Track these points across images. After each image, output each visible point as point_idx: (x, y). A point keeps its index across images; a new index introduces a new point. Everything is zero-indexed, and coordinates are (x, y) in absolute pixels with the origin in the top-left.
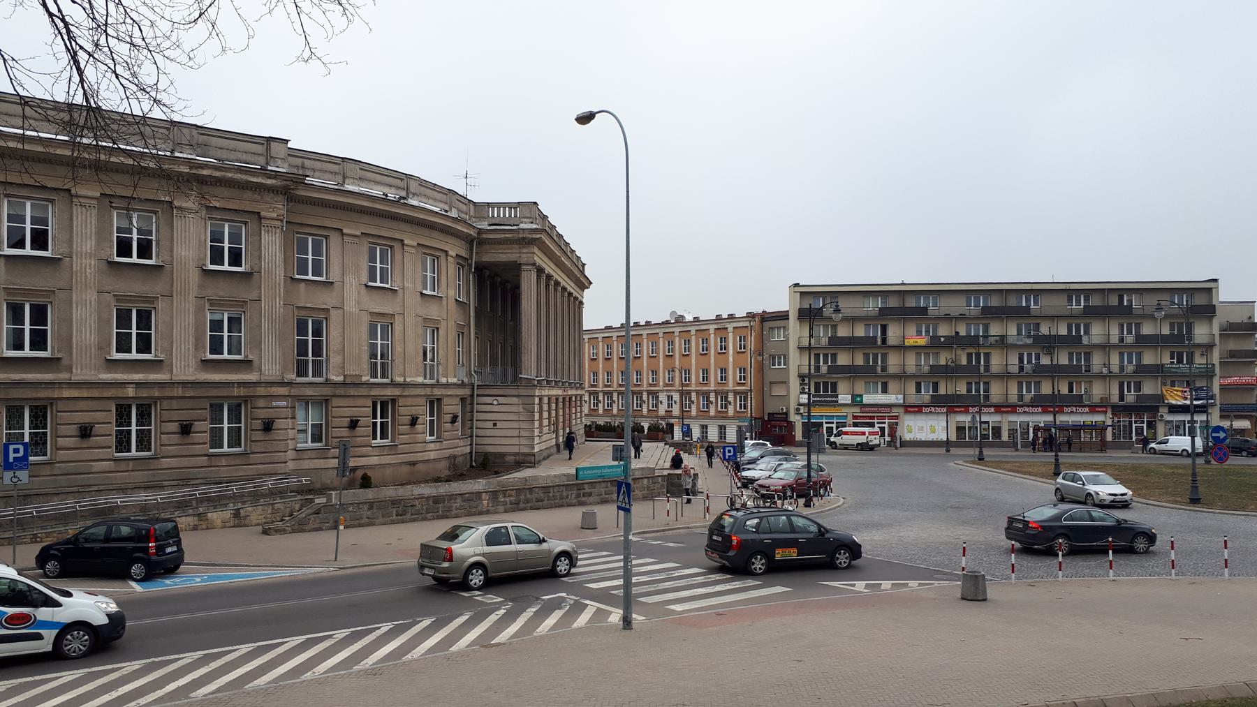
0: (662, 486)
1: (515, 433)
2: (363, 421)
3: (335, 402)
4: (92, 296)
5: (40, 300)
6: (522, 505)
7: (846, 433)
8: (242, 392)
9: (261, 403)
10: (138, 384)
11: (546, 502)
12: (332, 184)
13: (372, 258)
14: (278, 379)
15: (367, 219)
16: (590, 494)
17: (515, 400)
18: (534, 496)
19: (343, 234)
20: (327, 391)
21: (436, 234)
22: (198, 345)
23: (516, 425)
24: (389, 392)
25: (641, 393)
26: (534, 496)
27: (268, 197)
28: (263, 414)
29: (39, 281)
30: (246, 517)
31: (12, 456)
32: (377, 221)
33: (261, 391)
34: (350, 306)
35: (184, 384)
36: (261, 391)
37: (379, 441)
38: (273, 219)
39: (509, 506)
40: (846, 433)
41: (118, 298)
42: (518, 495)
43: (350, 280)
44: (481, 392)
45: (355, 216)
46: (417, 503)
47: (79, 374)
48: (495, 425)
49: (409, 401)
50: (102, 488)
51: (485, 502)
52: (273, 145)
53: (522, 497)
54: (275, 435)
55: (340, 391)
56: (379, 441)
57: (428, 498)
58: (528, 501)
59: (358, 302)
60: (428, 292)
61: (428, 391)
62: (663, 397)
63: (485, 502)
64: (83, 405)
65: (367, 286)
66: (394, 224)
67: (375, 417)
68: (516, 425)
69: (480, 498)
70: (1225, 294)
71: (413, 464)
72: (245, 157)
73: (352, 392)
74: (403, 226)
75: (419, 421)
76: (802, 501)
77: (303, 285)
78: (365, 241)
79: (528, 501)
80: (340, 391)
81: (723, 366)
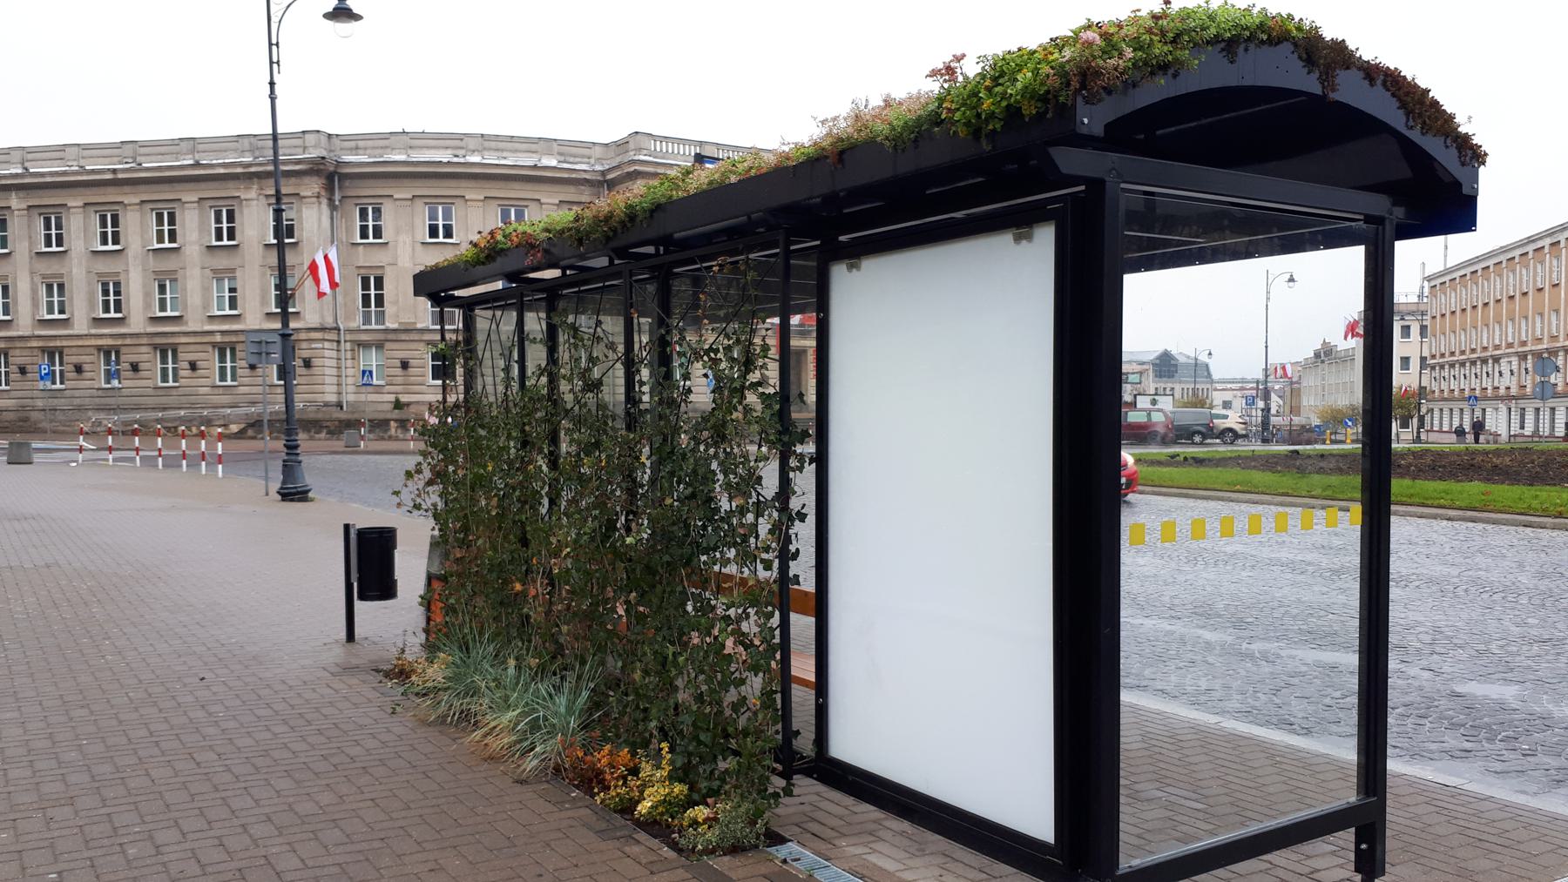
3: (388, 345)
4: (197, 272)
5: (379, 272)
9: (304, 345)
10: (223, 332)
12: (402, 158)
15: (142, 188)
21: (516, 185)
22: (92, 306)
27: (307, 180)
29: (169, 264)
32: (501, 184)
35: (195, 333)
41: (44, 276)
45: (406, 182)
47: (192, 326)
49: (17, 352)
54: (315, 370)
55: (391, 336)
64: (192, 348)
73: (403, 337)
74: (464, 183)
78: (419, 203)
80: (391, 336)
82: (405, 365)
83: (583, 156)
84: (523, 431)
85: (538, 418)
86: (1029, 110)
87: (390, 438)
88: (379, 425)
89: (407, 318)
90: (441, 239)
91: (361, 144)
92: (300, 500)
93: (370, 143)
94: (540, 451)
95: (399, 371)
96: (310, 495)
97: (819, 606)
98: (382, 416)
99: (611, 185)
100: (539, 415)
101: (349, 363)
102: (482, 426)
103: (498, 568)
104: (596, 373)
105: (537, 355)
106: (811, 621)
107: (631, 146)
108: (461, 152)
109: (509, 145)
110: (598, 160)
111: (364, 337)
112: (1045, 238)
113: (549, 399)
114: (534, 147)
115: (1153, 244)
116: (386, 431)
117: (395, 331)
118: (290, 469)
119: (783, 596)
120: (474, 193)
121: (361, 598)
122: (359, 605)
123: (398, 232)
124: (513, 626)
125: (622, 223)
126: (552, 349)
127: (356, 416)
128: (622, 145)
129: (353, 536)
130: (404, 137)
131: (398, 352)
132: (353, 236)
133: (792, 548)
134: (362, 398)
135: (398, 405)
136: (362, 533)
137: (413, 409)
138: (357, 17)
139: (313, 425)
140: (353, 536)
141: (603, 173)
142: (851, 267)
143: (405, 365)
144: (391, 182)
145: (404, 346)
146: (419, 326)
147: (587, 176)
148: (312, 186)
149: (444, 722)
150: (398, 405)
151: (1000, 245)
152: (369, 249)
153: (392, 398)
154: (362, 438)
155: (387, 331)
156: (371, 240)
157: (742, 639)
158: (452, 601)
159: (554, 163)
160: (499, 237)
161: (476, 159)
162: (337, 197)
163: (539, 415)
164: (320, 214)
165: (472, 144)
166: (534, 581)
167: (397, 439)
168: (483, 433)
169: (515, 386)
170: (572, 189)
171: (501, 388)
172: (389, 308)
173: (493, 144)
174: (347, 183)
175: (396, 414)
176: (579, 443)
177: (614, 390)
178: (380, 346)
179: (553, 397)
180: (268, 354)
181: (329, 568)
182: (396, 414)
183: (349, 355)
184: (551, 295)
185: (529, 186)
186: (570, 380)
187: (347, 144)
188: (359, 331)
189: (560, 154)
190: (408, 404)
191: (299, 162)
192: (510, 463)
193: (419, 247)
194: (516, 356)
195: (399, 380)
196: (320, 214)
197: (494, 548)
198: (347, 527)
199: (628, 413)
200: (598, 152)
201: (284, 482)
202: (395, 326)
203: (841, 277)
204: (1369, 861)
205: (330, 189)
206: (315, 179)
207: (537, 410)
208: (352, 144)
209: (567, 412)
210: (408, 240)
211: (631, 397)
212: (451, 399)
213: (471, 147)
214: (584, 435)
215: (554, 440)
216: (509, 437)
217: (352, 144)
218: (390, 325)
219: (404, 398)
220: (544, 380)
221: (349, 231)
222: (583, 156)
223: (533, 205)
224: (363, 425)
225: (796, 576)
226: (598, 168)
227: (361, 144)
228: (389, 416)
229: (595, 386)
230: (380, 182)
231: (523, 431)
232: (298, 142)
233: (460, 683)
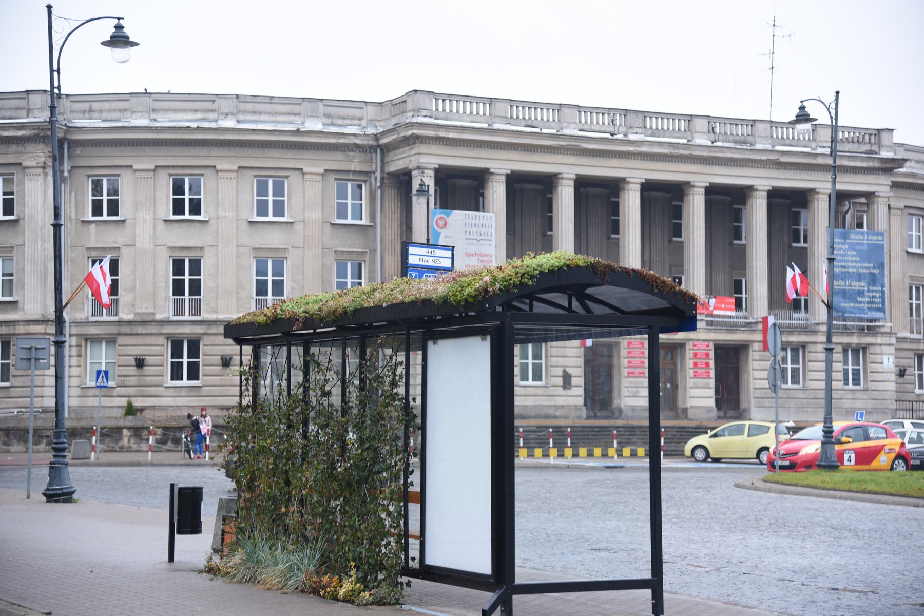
3: (121, 340)
7: (829, 363)
12: (144, 122)
13: (342, 194)
14: (38, 317)
19: (304, 174)
20: (113, 330)
21: (276, 153)
27: (30, 147)
32: (258, 152)
34: (144, 240)
37: (185, 382)
38: (34, 167)
40: (829, 363)
43: (145, 216)
45: (148, 150)
52: (31, 96)
56: (185, 382)
59: (154, 237)
60: (914, 250)
65: (907, 252)
66: (203, 151)
69: (121, 433)
70: (125, 30)
72: (8, 114)
73: (140, 330)
74: (215, 151)
76: (538, 452)
77: (93, 226)
82: (140, 363)
83: (353, 118)
84: (288, 419)
85: (299, 410)
86: (471, 300)
87: (122, 449)
88: (111, 434)
89: (144, 308)
90: (187, 216)
91: (96, 106)
92: (65, 501)
93: (107, 105)
94: (298, 431)
95: (133, 370)
96: (75, 496)
97: (421, 498)
98: (113, 423)
99: (385, 150)
100: (298, 410)
101: (74, 361)
102: (265, 417)
103: (272, 498)
104: (327, 388)
105: (297, 377)
106: (419, 506)
107: (409, 106)
108: (213, 116)
109: (268, 107)
110: (371, 121)
111: (93, 330)
112: (489, 338)
113: (304, 401)
114: (296, 109)
115: (569, 331)
116: (117, 441)
117: (130, 323)
118: (55, 471)
119: (405, 497)
120: (226, 162)
121: (179, 533)
122: (177, 537)
123: (137, 206)
124: (278, 528)
125: (341, 314)
126: (306, 373)
127: (84, 424)
128: (398, 105)
129: (176, 491)
130: (147, 99)
131: (132, 348)
132: (83, 214)
133: (410, 469)
134: (92, 402)
135: (131, 410)
136: (181, 490)
137: (148, 414)
138: (135, 44)
139: (39, 435)
140: (176, 491)
141: (376, 137)
142: (434, 343)
143: (140, 363)
144: (129, 150)
145: (140, 340)
146: (158, 317)
147: (358, 141)
148: (38, 155)
149: (241, 582)
150: (131, 410)
151: (477, 339)
152: (102, 227)
153: (123, 402)
154: (93, 448)
155: (120, 323)
156: (105, 217)
157: (389, 514)
158: (243, 525)
159: (318, 126)
160: (279, 311)
161: (230, 123)
162: (66, 167)
163: (298, 410)
164: (46, 187)
165: (225, 106)
166: (293, 505)
167: (129, 450)
168: (264, 421)
169: (285, 393)
170: (339, 155)
171: (276, 393)
172: (124, 295)
173: (249, 107)
174: (78, 151)
175: (130, 421)
176: (318, 424)
177: (336, 399)
178: (111, 341)
179: (306, 401)
180: (37, 359)
181: (160, 514)
182: (130, 421)
183: (74, 351)
184: (306, 341)
185: (290, 154)
186: (315, 391)
187: (78, 106)
188: (87, 323)
189: (328, 116)
190: (142, 410)
191: (21, 127)
192: (281, 438)
193: (161, 226)
194: (285, 376)
195: (133, 380)
196: (46, 187)
197: (270, 487)
198: (172, 486)
199: (343, 408)
200: (371, 112)
201: (50, 484)
202: (130, 317)
203: (430, 344)
204: (658, 606)
205: (57, 159)
206: (41, 146)
207: (296, 407)
208: (86, 106)
209: (313, 408)
210: (149, 217)
211: (345, 400)
212: (244, 403)
213: (225, 111)
214: (322, 420)
215: (306, 424)
216: (281, 423)
217: (86, 106)
218: (125, 315)
219: (138, 403)
220: (301, 390)
221: (79, 206)
222: (353, 118)
223: (294, 176)
224: (94, 433)
225: (412, 482)
226: (371, 131)
227: (96, 106)
228: (121, 423)
229: (327, 394)
230: (117, 151)
231: (288, 419)
232: (23, 103)
233: (253, 561)
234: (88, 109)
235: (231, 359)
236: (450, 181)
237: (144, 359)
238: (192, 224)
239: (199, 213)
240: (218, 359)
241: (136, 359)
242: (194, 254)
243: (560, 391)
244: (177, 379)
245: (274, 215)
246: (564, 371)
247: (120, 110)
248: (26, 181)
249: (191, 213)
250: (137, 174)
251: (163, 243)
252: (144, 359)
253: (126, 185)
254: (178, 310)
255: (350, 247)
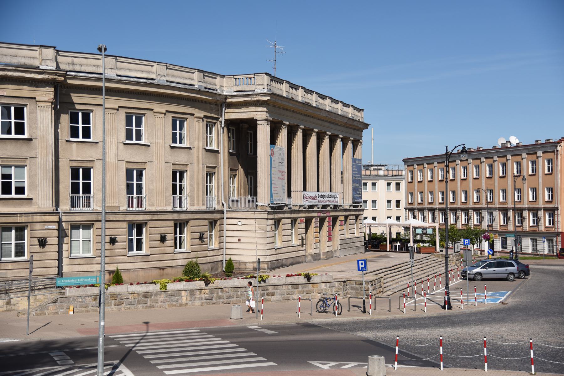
0: (339, 290)
1: (253, 246)
2: (169, 237)
6: (214, 300)
8: (24, 219)
9: (38, 226)
11: (235, 299)
16: (273, 294)
17: (253, 222)
18: (225, 294)
23: (253, 240)
24: (141, 217)
25: (538, 210)
26: (225, 294)
28: (40, 234)
30: (14, 305)
31: (361, 266)
33: (38, 218)
34: (111, 158)
36: (38, 218)
37: (135, 252)
39: (204, 301)
42: (211, 293)
44: (229, 215)
46: (130, 296)
48: (239, 240)
50: (47, 286)
51: (184, 298)
53: (215, 295)
56: (135, 252)
57: (138, 293)
58: (219, 298)
61: (176, 216)
62: (485, 214)
63: (184, 298)
67: (176, 234)
68: (253, 240)
69: (180, 295)
71: (163, 268)
75: (204, 236)
77: (75, 144)
79: (219, 298)
81: (550, 186)
195: (108, 253)
234: (71, 62)
235: (45, 239)
236: (241, 125)
237: (116, 238)
238: (175, 149)
239: (140, 140)
240: (158, 237)
241: (39, 240)
242: (88, 165)
243: (300, 248)
244: (19, 256)
245: (16, 134)
246: (203, 241)
247: (94, 66)
248: (39, 111)
249: (84, 137)
250: (155, 114)
251: (123, 159)
252: (116, 238)
253: (96, 119)
254: (130, 204)
255: (211, 164)
